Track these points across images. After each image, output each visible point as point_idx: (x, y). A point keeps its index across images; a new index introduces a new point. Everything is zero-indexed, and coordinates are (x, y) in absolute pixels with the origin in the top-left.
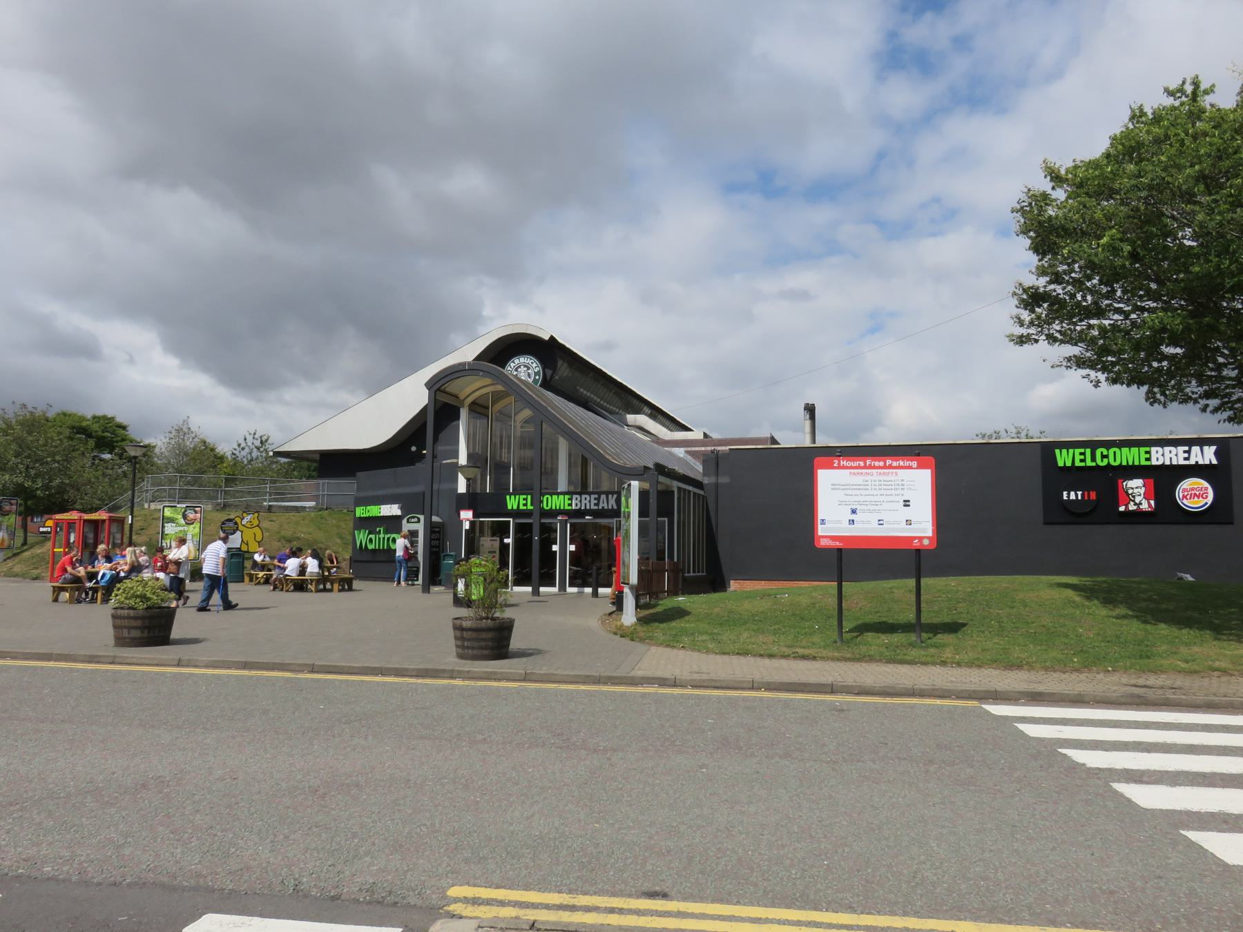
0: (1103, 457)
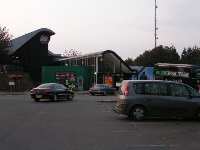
0: (162, 73)
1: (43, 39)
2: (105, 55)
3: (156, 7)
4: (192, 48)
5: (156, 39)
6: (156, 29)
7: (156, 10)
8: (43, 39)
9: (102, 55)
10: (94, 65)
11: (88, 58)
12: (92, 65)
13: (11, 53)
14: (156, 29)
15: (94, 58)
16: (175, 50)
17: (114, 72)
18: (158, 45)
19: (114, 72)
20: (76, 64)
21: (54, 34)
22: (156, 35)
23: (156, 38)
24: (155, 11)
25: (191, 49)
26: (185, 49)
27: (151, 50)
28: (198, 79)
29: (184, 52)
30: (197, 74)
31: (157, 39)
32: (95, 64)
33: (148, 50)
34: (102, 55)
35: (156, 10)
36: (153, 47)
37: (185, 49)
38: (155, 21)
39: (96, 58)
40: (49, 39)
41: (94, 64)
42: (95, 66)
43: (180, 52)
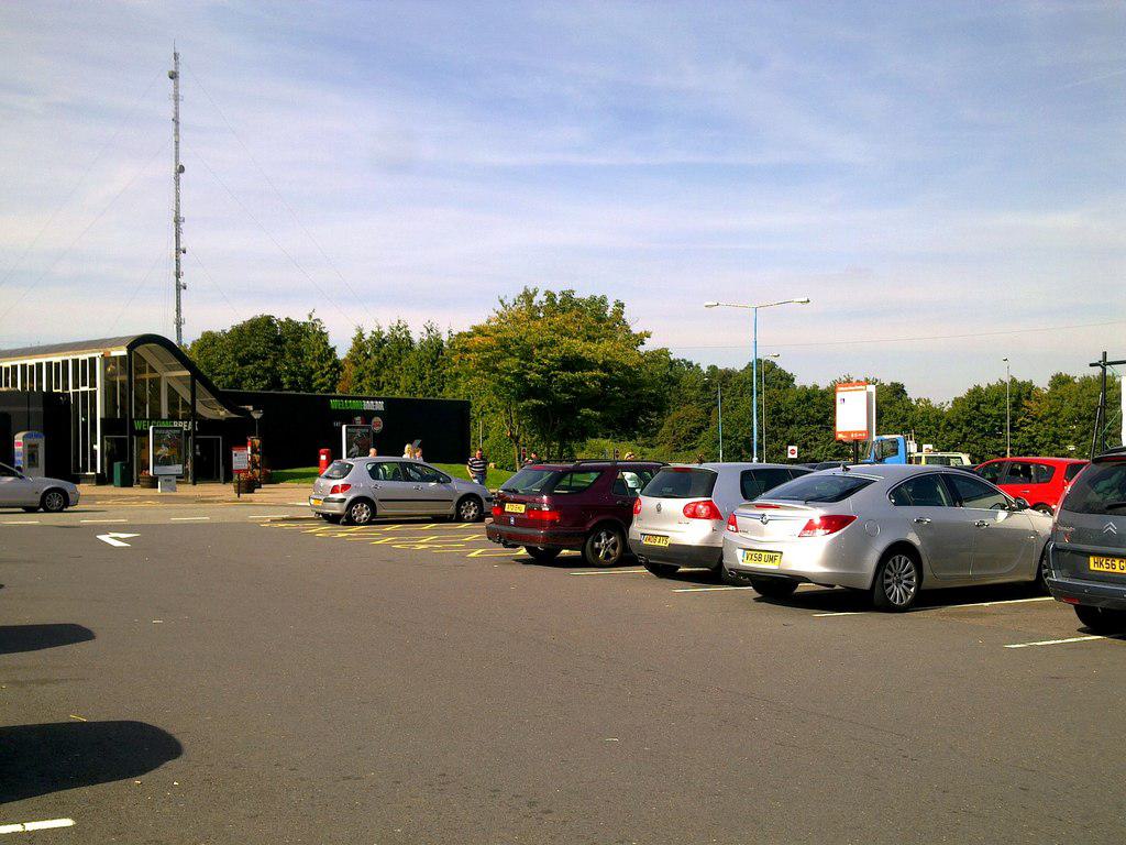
2: (140, 350)
3: (182, 169)
4: (386, 332)
5: (178, 290)
7: (177, 180)
8: (898, 409)
9: (124, 352)
10: (87, 388)
12: (76, 386)
15: (84, 362)
20: (7, 385)
22: (178, 275)
25: (383, 336)
26: (361, 335)
28: (793, 461)
30: (44, 390)
31: (182, 290)
32: (93, 384)
33: (216, 329)
34: (124, 352)
35: (177, 180)
38: (178, 221)
39: (98, 360)
41: (84, 384)
42: (94, 394)
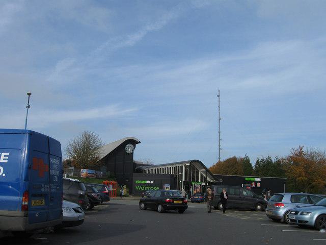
1: (129, 148)
6: (220, 140)
11: (174, 166)
13: (102, 158)
14: (220, 140)
16: (248, 161)
17: (200, 181)
18: (224, 158)
19: (200, 181)
21: (139, 142)
23: (220, 149)
24: (218, 124)
26: (258, 160)
27: (274, 160)
29: (258, 163)
32: (182, 173)
36: (217, 161)
37: (258, 160)
40: (135, 147)
43: (253, 163)
